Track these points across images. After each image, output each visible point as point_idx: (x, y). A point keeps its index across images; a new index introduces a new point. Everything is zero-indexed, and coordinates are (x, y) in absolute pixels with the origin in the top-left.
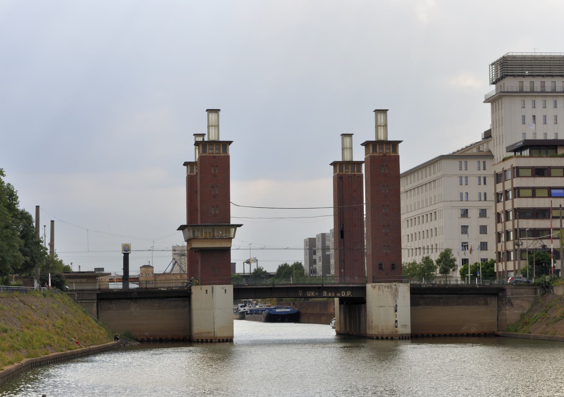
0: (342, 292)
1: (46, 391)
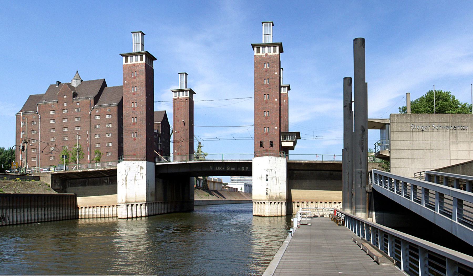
0: (242, 168)
1: (124, 263)
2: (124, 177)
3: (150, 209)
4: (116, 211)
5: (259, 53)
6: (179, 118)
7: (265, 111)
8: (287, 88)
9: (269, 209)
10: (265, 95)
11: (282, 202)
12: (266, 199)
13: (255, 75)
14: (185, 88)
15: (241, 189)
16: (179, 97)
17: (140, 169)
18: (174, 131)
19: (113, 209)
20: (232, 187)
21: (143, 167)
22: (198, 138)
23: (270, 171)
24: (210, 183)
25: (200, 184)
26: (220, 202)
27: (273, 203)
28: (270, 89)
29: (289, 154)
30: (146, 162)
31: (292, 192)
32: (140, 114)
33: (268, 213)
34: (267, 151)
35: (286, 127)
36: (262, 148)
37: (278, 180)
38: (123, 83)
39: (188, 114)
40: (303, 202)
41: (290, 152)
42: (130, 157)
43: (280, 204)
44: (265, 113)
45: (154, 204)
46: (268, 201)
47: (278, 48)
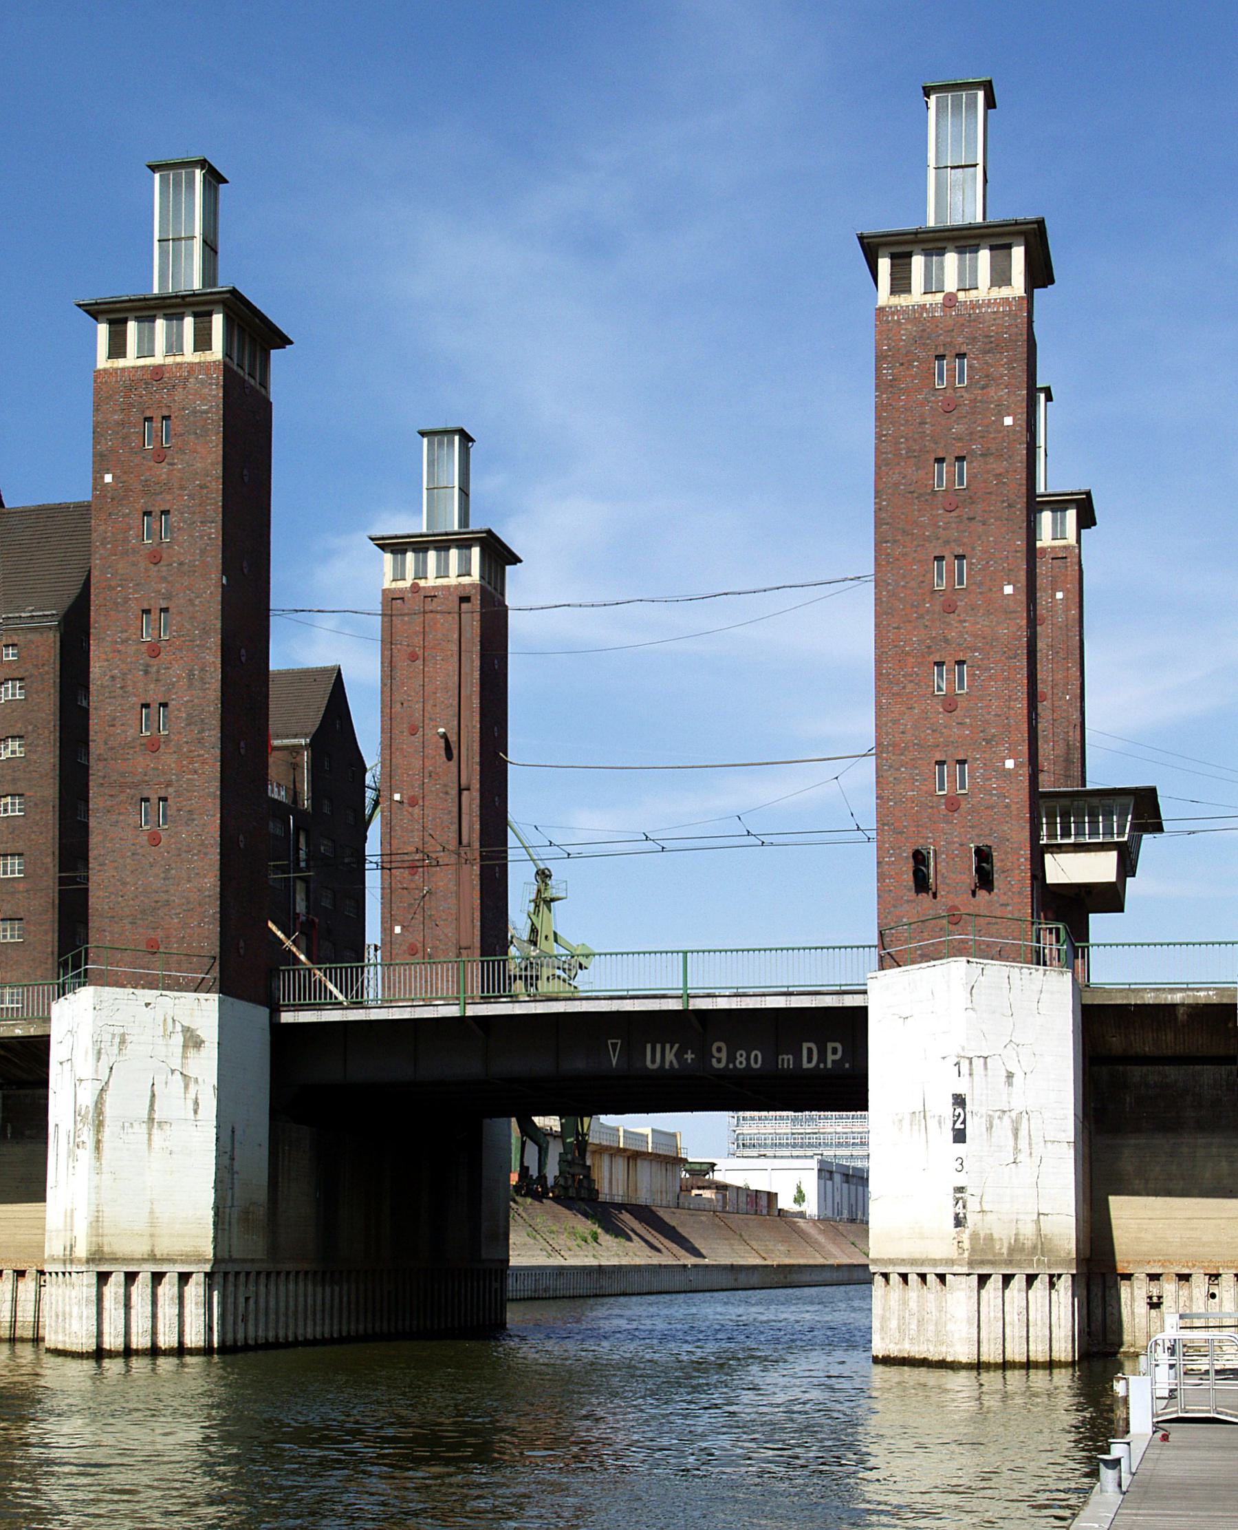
0: (805, 1046)
2: (87, 1098)
3: (236, 1308)
4: (31, 1307)
5: (908, 290)
6: (418, 715)
7: (940, 664)
8: (1071, 515)
9: (969, 1320)
10: (939, 558)
11: (1051, 1276)
12: (955, 1255)
13: (879, 436)
14: (456, 528)
15: (800, 1198)
16: (422, 583)
17: (185, 1047)
18: (385, 793)
19: (15, 1290)
20: (741, 1184)
21: (203, 1036)
22: (533, 838)
23: (978, 1063)
24: (606, 1160)
25: (542, 1164)
26: (666, 1282)
27: (995, 1283)
28: (970, 519)
29: (1092, 939)
30: (221, 1002)
31: (1113, 1213)
32: (190, 686)
33: (969, 1340)
34: (955, 918)
35: (1068, 761)
36: (923, 896)
37: (1023, 1133)
38: (95, 489)
39: (477, 689)
40: (1184, 1278)
41: (1099, 924)
42: (128, 956)
43: (1040, 1284)
44: (940, 675)
45: (263, 1279)
46: (965, 1270)
47: (1018, 254)
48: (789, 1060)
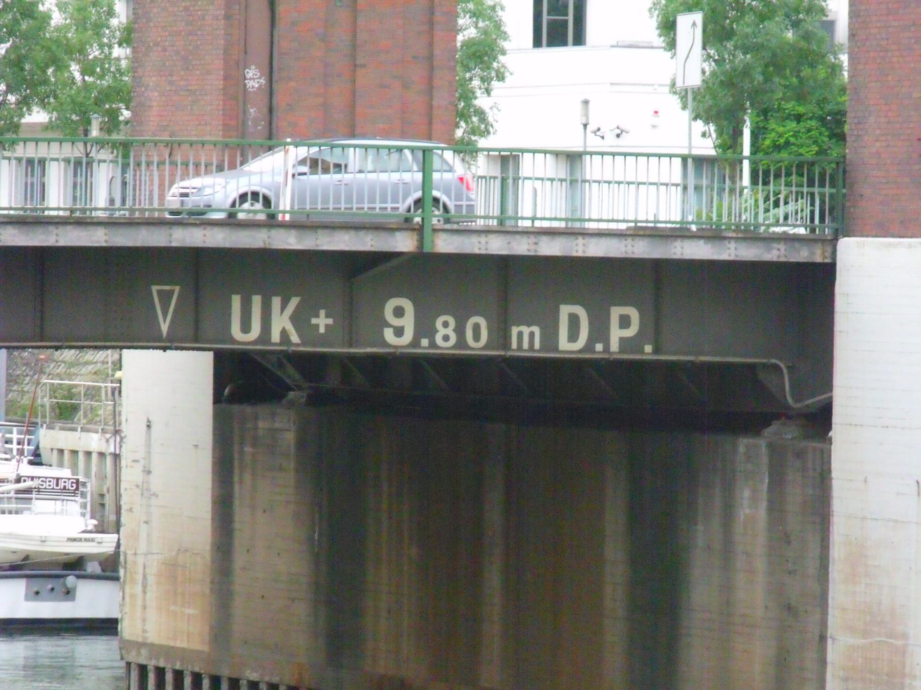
0: (565, 310)
48: (532, 335)
